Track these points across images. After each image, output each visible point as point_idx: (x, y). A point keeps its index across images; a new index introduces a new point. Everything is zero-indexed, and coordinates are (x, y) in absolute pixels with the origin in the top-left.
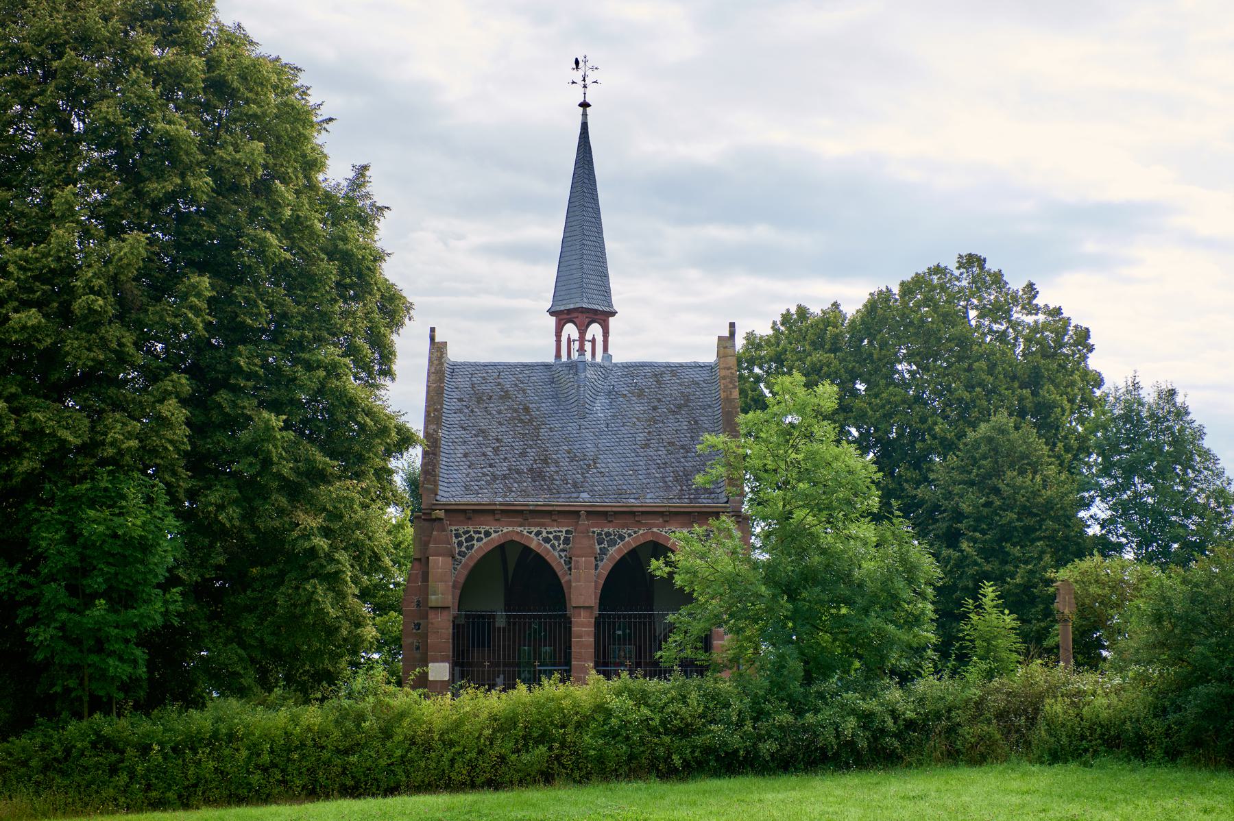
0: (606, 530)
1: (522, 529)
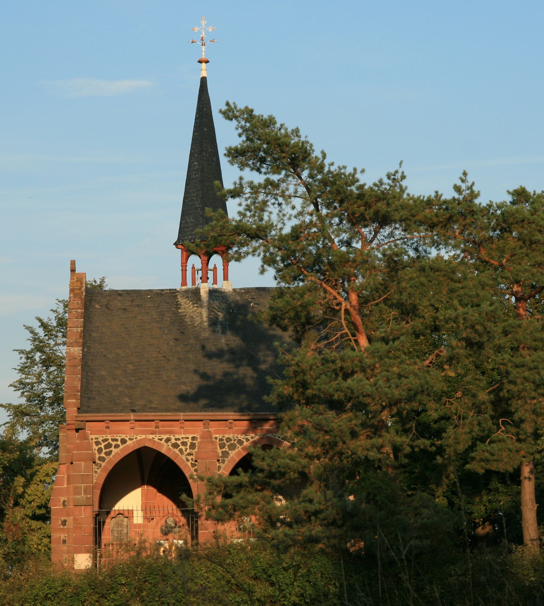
0: (227, 436)
1: (153, 436)
